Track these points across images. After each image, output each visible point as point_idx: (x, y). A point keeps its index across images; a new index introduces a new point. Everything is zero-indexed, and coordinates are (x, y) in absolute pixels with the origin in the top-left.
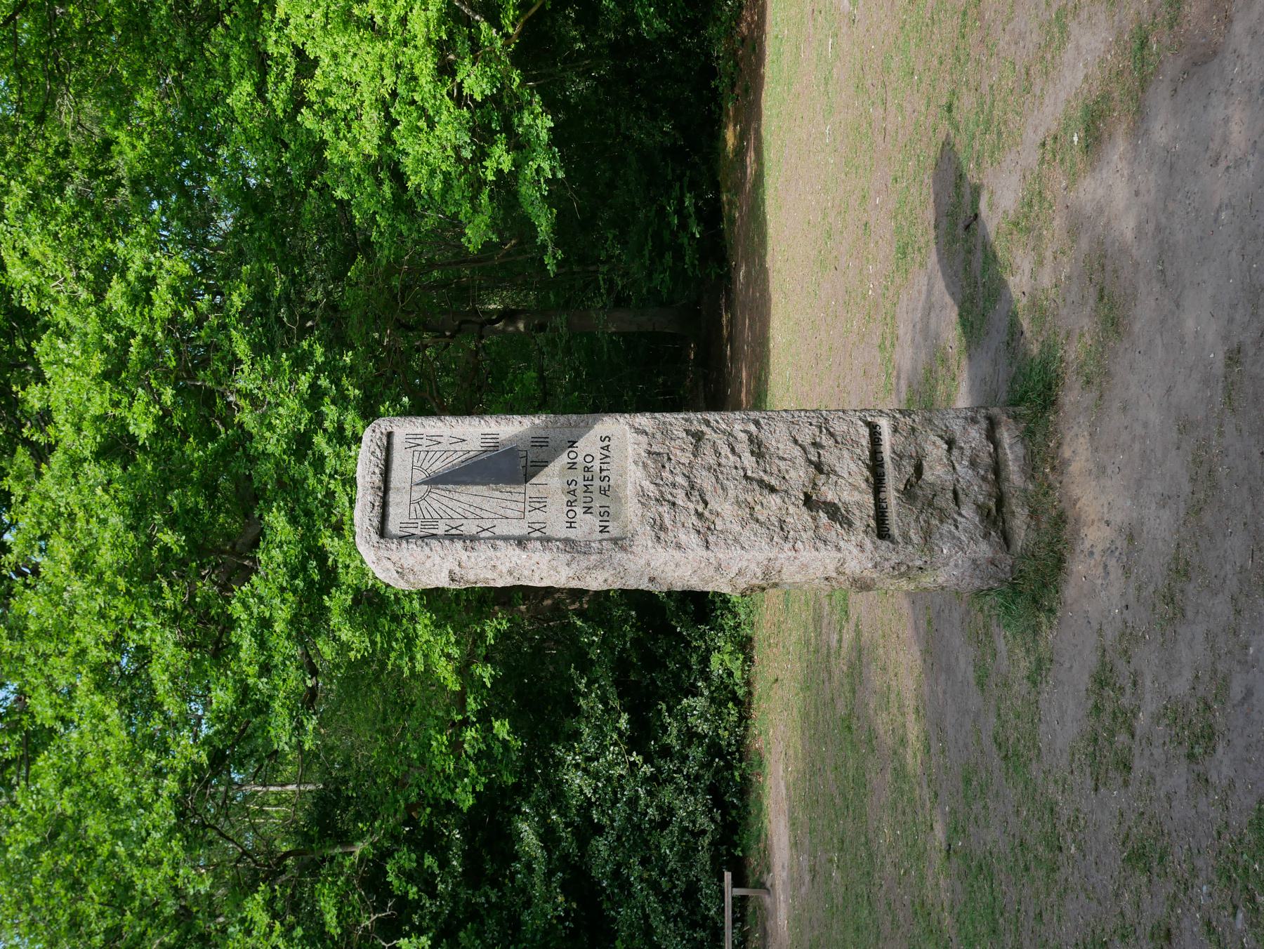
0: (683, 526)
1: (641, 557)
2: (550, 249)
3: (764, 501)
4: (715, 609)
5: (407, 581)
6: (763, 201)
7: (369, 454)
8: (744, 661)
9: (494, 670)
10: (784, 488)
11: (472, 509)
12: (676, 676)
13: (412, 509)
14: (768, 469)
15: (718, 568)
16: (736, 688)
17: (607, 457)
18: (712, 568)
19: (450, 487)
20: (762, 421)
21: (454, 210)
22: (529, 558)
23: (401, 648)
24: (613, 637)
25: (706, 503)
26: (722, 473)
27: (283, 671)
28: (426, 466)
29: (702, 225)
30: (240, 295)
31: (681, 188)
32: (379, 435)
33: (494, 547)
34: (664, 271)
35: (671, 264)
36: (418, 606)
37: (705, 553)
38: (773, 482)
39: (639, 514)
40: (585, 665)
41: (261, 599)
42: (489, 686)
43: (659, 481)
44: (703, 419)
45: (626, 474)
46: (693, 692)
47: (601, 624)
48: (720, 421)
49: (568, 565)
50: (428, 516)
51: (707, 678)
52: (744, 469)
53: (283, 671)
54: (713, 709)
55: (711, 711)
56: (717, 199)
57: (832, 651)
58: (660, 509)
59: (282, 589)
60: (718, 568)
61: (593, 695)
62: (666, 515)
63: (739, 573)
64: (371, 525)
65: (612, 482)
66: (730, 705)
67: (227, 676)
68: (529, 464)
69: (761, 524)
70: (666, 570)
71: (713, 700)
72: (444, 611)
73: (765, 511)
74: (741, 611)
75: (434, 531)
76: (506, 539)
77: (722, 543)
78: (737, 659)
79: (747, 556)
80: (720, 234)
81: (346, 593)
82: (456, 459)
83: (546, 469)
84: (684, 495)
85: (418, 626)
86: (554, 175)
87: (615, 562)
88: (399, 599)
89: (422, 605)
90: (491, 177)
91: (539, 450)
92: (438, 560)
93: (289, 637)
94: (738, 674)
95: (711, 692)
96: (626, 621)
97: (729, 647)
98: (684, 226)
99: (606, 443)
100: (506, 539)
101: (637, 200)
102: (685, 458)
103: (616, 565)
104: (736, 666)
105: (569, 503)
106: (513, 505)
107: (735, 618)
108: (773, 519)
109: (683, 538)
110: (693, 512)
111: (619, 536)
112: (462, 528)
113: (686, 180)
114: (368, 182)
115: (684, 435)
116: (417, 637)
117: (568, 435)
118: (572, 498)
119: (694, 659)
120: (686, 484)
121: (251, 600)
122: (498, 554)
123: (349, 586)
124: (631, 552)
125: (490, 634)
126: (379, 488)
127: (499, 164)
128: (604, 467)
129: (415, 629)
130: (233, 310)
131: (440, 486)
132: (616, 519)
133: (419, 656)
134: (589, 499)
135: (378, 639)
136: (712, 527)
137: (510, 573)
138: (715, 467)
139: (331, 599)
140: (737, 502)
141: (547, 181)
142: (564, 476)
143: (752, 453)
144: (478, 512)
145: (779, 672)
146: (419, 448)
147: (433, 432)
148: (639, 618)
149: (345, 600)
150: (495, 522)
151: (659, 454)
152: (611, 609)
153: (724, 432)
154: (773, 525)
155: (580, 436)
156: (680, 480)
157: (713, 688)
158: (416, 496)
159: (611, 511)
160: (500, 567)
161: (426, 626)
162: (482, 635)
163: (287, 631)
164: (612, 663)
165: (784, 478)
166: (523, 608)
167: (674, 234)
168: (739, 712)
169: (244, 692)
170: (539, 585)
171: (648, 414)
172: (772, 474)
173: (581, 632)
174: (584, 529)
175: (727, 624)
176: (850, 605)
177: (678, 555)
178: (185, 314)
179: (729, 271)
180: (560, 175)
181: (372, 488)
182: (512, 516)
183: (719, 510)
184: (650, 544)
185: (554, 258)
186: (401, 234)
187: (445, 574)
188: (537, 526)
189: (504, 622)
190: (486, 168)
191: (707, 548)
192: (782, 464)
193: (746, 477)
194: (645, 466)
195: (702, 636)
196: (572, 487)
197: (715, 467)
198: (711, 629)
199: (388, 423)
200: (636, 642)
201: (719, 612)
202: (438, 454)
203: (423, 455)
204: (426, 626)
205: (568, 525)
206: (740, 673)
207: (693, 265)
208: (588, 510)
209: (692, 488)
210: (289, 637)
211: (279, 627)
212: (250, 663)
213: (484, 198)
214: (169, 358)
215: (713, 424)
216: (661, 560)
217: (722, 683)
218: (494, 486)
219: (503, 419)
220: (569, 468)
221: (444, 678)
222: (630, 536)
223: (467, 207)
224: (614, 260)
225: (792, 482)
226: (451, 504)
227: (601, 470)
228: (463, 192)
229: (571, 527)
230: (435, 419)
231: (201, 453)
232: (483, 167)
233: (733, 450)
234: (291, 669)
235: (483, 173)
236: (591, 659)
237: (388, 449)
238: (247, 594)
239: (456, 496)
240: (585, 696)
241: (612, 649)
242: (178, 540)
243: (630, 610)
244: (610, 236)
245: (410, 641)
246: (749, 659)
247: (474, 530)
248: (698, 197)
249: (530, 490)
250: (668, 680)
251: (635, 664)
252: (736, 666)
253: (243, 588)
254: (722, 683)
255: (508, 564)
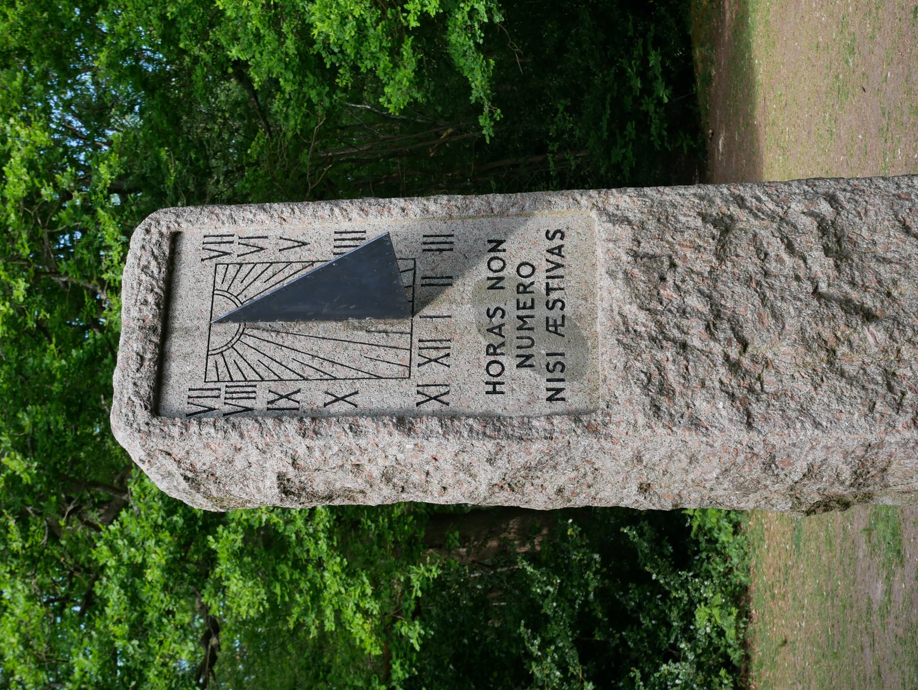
0: (703, 385)
1: (624, 445)
2: (486, 110)
3: (855, 338)
4: (699, 552)
5: (208, 496)
6: (748, 46)
7: (137, 271)
8: (739, 617)
9: (424, 629)
10: (890, 312)
11: (316, 363)
12: (652, 635)
13: (211, 364)
14: (858, 279)
15: (770, 464)
16: (729, 651)
17: (558, 266)
18: (758, 466)
19: (278, 325)
20: (841, 196)
21: (369, 64)
22: (419, 449)
23: (305, 602)
24: (572, 586)
25: (745, 345)
26: (771, 287)
27: (160, 631)
28: (235, 290)
29: (671, 88)
30: (110, 166)
31: (645, 46)
32: (155, 237)
33: (355, 430)
34: (625, 145)
35: (633, 136)
36: (325, 547)
37: (745, 437)
38: (869, 302)
39: (620, 366)
40: (538, 623)
41: (132, 542)
42: (418, 648)
43: (654, 305)
44: (732, 194)
45: (594, 295)
46: (674, 655)
47: (557, 571)
48: (764, 198)
49: (490, 461)
50: (237, 376)
51: (691, 639)
52: (813, 281)
53: (160, 631)
54: (700, 678)
55: (698, 680)
56: (689, 57)
57: (875, 607)
58: (660, 356)
59: (156, 528)
60: (770, 464)
61: (549, 660)
62: (670, 366)
63: (810, 473)
64: (137, 393)
65: (568, 311)
66: (723, 672)
67: (91, 637)
68: (419, 281)
69: (851, 380)
70: (672, 468)
71: (700, 666)
72: (364, 554)
73: (856, 357)
74: (733, 552)
75: (248, 403)
76: (376, 415)
77: (777, 416)
78: (730, 614)
79: (825, 440)
80: (692, 98)
81: (236, 532)
82: (287, 276)
83: (449, 291)
84: (702, 328)
85: (326, 574)
86: (491, 18)
87: (577, 454)
88: (302, 539)
89: (330, 547)
90: (414, 24)
91: (437, 257)
92: (254, 456)
93: (165, 588)
94: (731, 633)
95: (698, 656)
96: (588, 567)
97: (719, 599)
98: (648, 90)
99: (557, 242)
100: (376, 415)
101: (591, 63)
102: (702, 263)
103: (578, 462)
104: (728, 623)
105: (492, 350)
106: (390, 355)
107: (725, 561)
108: (872, 369)
109: (702, 406)
110: (720, 360)
111: (582, 406)
112: (298, 397)
113: (651, 34)
114: (269, 36)
115: (699, 222)
116: (325, 587)
117: (487, 229)
118: (496, 340)
119: (674, 614)
120: (706, 310)
121: (120, 542)
122: (363, 442)
123: (239, 523)
124: (608, 436)
125: (416, 584)
126: (154, 329)
127: (423, 6)
128: (554, 283)
129: (322, 577)
130: (101, 186)
131: (261, 324)
132: (578, 375)
133: (329, 612)
134: (526, 342)
135: (278, 590)
136: (758, 387)
137: (387, 478)
138: (759, 277)
139: (217, 540)
140: (803, 339)
141: (483, 26)
142: (481, 301)
143: (827, 251)
144: (327, 368)
145: (788, 632)
146: (226, 259)
147: (250, 230)
148: (604, 563)
149: (235, 541)
150: (358, 385)
151: (653, 257)
152: (569, 552)
153: (772, 217)
154: (873, 381)
155: (509, 231)
156: (694, 302)
157: (699, 651)
158: (217, 341)
159: (569, 361)
160: (368, 467)
161: (335, 574)
162: (408, 585)
163: (162, 581)
164: (572, 619)
165: (889, 294)
166: (463, 550)
167: (637, 101)
168: (734, 682)
169: (110, 653)
170: (442, 501)
171: (630, 190)
172: (866, 288)
173: (533, 581)
174: (517, 394)
175: (715, 569)
176: (905, 542)
177: (694, 440)
178: (43, 191)
179: (704, 142)
180: (498, 19)
181: (141, 328)
182: (388, 373)
183: (770, 355)
184: (641, 419)
185: (492, 118)
186: (309, 101)
187: (271, 481)
188: (433, 391)
189: (434, 569)
190: (408, 12)
191: (749, 425)
192: (885, 272)
193: (816, 293)
194: (629, 278)
195: (683, 585)
196: (496, 320)
197: (759, 277)
198: (695, 576)
199: (173, 218)
200: (601, 593)
201: (704, 555)
202: (259, 269)
203: (232, 270)
204: (335, 574)
205: (490, 388)
206: (733, 631)
207: (660, 136)
208: (525, 362)
209: (718, 316)
210: (165, 588)
211: (153, 575)
212: (119, 621)
213: (406, 49)
214: (22, 244)
215: (751, 202)
216: (663, 451)
217: (710, 643)
218: (356, 322)
219: (372, 204)
220: (492, 287)
221: (362, 641)
222: (603, 405)
223: (385, 60)
224: (566, 136)
225: (905, 303)
226: (279, 355)
227: (549, 290)
228: (381, 43)
229: (495, 392)
230: (254, 208)
231: (63, 362)
232: (404, 10)
233: (790, 247)
234: (168, 628)
235: (405, 18)
236: (546, 615)
237: (172, 262)
238: (115, 535)
239: (289, 341)
240: (539, 660)
241: (572, 602)
242: (29, 467)
243: (593, 552)
244: (561, 108)
245: (317, 593)
246: (744, 614)
247: (320, 399)
248: (665, 55)
249: (422, 328)
250: (642, 640)
251: (601, 620)
252: (728, 623)
253: (111, 527)
254: (710, 643)
255: (381, 462)
